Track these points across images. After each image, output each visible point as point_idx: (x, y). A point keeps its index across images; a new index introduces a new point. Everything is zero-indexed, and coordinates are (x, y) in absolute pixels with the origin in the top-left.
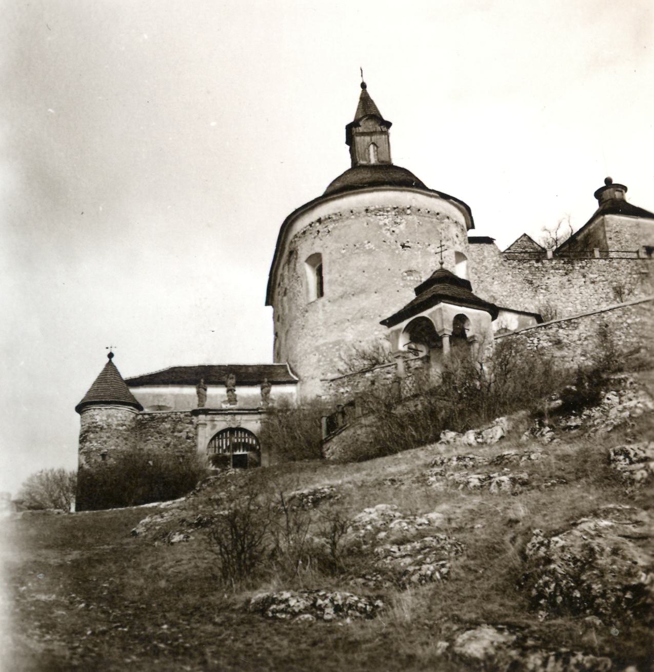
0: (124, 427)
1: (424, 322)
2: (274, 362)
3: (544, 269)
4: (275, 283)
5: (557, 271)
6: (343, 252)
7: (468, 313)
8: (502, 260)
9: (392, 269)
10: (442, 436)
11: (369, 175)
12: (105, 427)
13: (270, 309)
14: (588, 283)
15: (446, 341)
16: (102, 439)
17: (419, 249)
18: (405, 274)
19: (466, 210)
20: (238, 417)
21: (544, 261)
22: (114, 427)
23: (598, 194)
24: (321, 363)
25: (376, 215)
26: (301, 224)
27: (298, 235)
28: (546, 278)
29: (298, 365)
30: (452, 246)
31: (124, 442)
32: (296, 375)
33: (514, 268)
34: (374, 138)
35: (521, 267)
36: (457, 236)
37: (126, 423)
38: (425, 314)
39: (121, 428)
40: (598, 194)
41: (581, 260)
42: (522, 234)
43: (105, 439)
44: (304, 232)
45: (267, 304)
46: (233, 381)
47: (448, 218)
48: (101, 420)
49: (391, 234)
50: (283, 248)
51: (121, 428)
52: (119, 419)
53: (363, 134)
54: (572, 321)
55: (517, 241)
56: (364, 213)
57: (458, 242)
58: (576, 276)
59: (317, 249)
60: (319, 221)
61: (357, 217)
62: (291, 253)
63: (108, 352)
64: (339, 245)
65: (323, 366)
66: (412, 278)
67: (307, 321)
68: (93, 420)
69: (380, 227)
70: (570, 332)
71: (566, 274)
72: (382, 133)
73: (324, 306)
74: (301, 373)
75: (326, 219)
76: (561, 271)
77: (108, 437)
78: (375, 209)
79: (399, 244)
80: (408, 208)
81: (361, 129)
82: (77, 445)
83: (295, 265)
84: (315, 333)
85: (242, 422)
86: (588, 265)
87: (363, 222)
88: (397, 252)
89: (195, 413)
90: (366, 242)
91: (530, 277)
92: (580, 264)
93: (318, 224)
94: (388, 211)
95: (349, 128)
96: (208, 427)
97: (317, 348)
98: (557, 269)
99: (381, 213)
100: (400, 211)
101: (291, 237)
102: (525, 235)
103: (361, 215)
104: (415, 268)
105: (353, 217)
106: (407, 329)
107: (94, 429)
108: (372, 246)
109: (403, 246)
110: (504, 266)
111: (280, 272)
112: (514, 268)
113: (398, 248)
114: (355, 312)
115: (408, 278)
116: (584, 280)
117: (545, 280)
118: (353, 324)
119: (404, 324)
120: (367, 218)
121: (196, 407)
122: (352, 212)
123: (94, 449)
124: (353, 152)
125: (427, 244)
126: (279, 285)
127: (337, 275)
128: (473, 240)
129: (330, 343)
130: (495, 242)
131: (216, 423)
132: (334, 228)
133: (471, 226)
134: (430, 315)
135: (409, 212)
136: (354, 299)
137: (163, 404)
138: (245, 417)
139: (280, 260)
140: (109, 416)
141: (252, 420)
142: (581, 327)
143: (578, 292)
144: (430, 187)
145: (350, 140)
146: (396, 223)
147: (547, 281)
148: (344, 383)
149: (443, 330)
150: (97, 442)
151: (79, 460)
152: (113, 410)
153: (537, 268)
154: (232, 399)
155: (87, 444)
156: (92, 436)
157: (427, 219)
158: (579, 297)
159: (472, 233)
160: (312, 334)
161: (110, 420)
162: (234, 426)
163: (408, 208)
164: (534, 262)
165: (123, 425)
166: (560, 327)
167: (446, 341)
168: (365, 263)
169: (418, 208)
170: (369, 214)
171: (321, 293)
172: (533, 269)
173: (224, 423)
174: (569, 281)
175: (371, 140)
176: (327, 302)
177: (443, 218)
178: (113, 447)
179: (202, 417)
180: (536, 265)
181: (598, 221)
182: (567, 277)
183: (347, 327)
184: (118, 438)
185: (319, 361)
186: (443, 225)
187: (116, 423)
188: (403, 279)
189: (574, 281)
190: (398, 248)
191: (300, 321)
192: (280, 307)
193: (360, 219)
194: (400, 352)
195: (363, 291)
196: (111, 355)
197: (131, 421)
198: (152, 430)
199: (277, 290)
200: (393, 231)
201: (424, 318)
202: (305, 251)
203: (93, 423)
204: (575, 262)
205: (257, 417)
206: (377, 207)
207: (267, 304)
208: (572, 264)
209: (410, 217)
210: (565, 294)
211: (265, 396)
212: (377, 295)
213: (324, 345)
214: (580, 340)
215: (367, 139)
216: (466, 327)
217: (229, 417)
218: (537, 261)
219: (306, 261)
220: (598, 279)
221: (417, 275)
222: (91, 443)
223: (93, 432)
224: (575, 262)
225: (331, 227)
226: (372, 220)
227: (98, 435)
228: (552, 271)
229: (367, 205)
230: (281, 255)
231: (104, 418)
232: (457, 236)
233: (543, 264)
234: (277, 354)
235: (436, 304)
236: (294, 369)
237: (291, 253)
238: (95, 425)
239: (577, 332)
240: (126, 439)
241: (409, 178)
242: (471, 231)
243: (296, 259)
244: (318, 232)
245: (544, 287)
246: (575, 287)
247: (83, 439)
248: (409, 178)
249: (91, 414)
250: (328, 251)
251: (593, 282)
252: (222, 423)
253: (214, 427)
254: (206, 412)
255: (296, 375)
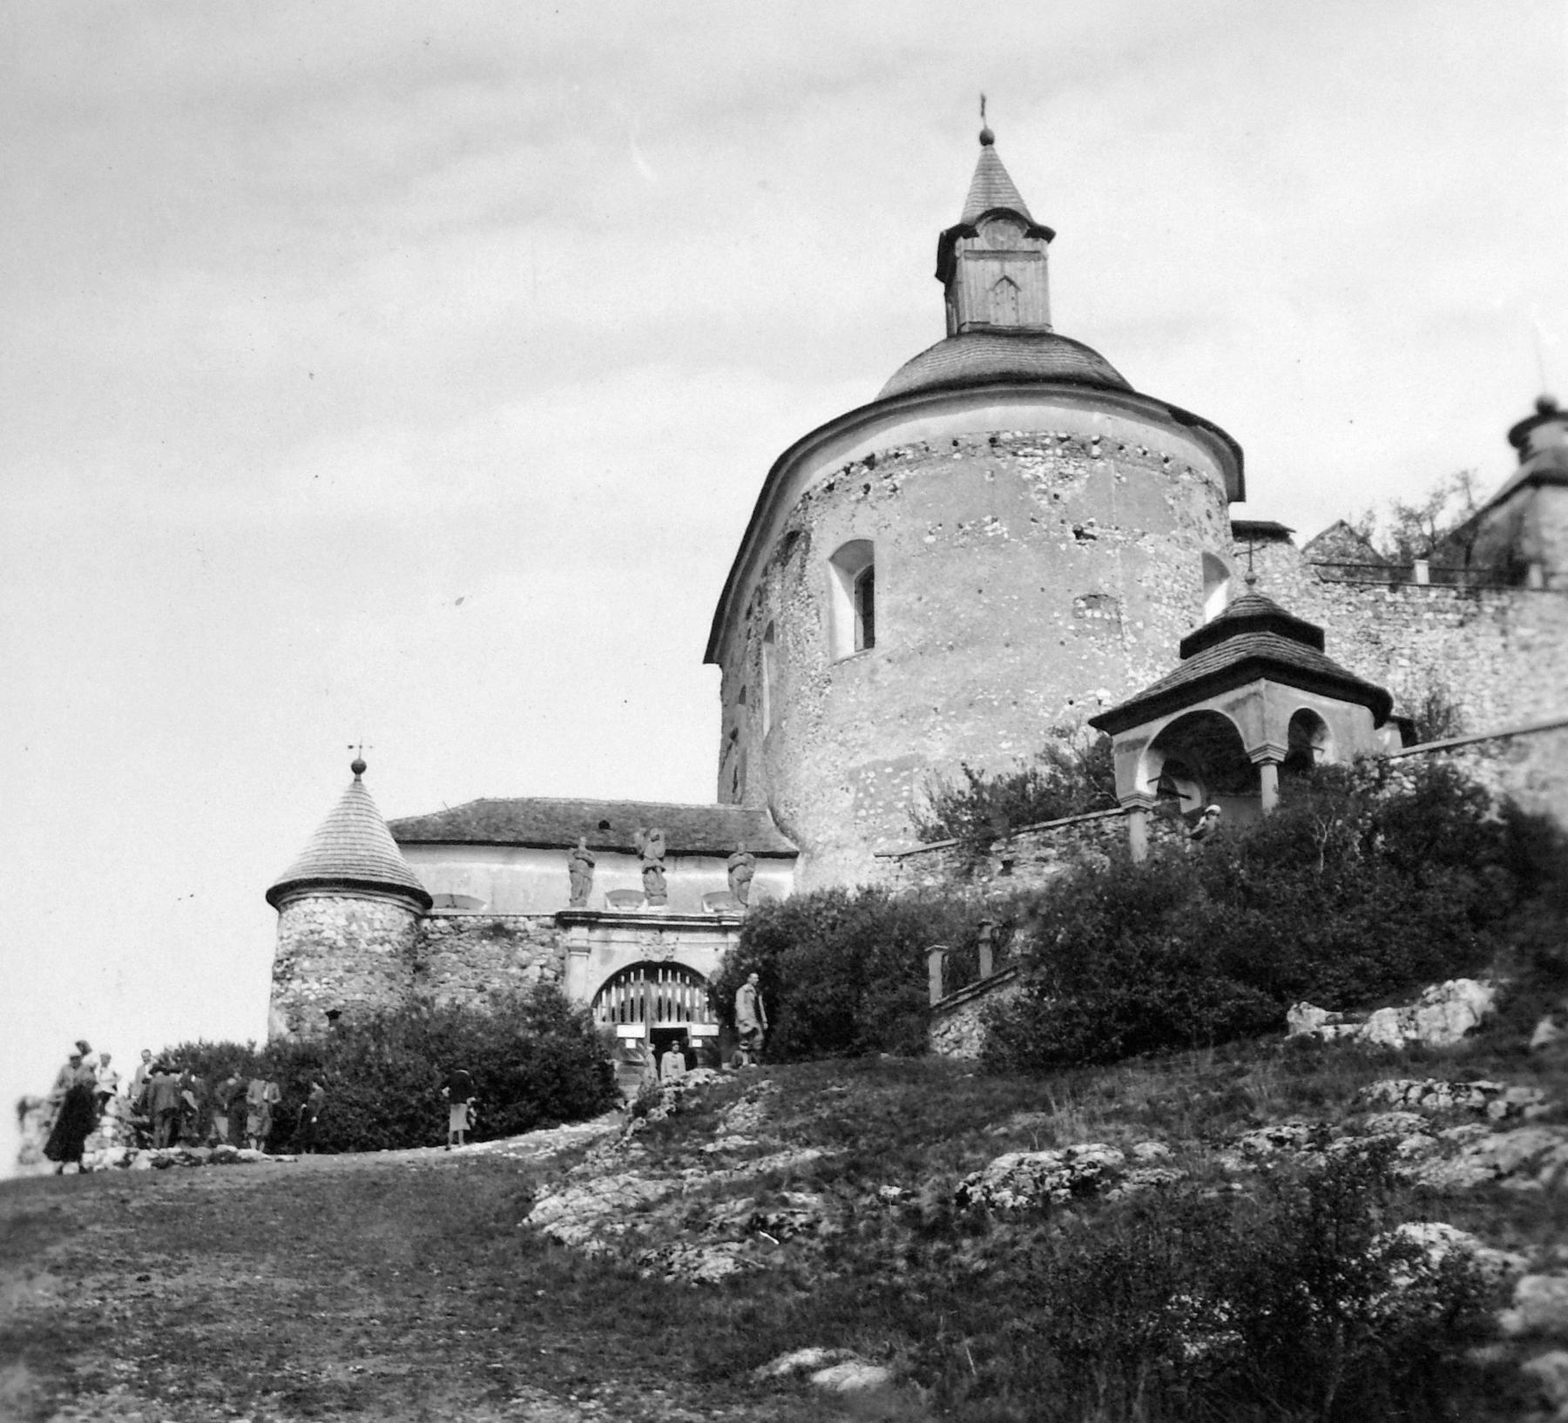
0: (388, 947)
1: (1205, 724)
2: (720, 800)
3: (1409, 609)
4: (735, 609)
5: (1441, 617)
6: (930, 539)
7: (1320, 708)
8: (1308, 581)
9: (1049, 588)
10: (1292, 1017)
11: (1000, 355)
12: (342, 943)
13: (714, 671)
14: (1513, 649)
15: (1270, 776)
16: (333, 974)
17: (1117, 542)
18: (1082, 604)
19: (1230, 455)
20: (669, 937)
21: (1409, 590)
22: (363, 945)
23: (1519, 437)
24: (863, 813)
25: (1015, 454)
26: (820, 472)
27: (814, 494)
28: (1413, 629)
29: (801, 813)
30: (1196, 539)
31: (387, 984)
32: (795, 838)
33: (1336, 601)
34: (1011, 268)
35: (1353, 600)
36: (1209, 517)
37: (394, 936)
38: (1215, 704)
39: (378, 949)
40: (1519, 437)
41: (1499, 590)
42: (1334, 521)
43: (340, 973)
44: (830, 487)
45: (708, 659)
46: (660, 848)
47: (1189, 470)
48: (336, 928)
49: (1051, 503)
50: (766, 529)
51: (378, 949)
52: (377, 925)
53: (981, 254)
54: (1515, 739)
55: (1321, 537)
56: (986, 447)
57: (1212, 532)
58: (1483, 630)
59: (863, 531)
60: (870, 462)
61: (968, 456)
62: (792, 537)
63: (353, 757)
64: (919, 523)
65: (865, 819)
66: (1097, 614)
67: (828, 704)
68: (313, 927)
69: (1025, 485)
70: (1507, 767)
71: (1462, 624)
72: (1037, 255)
73: (874, 671)
74: (800, 828)
75: (887, 458)
76: (1450, 616)
77: (349, 971)
78: (1015, 440)
79: (1069, 529)
80: (1095, 443)
81: (979, 243)
82: (267, 985)
83: (803, 567)
84: (850, 735)
85: (679, 948)
86: (1516, 606)
87: (982, 470)
88: (1063, 547)
89: (564, 921)
90: (988, 519)
91: (1374, 628)
92: (1496, 603)
93: (866, 470)
94: (1044, 447)
95: (948, 242)
96: (595, 957)
97: (853, 776)
98: (1440, 611)
99: (1029, 450)
100: (1075, 447)
101: (794, 497)
102: (1342, 524)
103: (979, 453)
104: (1106, 588)
105: (957, 456)
106: (1160, 744)
107: (310, 948)
108: (1002, 529)
109: (1079, 534)
110: (1313, 597)
111: (755, 579)
112: (1336, 601)
113: (1065, 539)
114: (951, 693)
115: (1089, 613)
116: (1502, 640)
117: (1409, 635)
118: (948, 719)
119: (1157, 727)
120: (990, 459)
121: (564, 906)
122: (955, 443)
123: (312, 997)
124: (950, 295)
125: (1138, 531)
126: (749, 613)
127: (912, 597)
128: (1243, 531)
129: (886, 764)
130: (1292, 536)
131: (613, 946)
132: (908, 481)
133: (1237, 492)
134: (1232, 707)
135: (1096, 450)
136: (952, 658)
137: (463, 892)
138: (686, 937)
139: (755, 553)
140: (351, 917)
141: (707, 945)
142: (1535, 759)
143: (1487, 668)
144: (1138, 389)
145: (947, 270)
146: (1063, 476)
147: (1415, 639)
148: (933, 865)
149: (1264, 749)
150: (319, 980)
151: (270, 1021)
152: (363, 903)
153: (1393, 604)
154: (656, 894)
155: (296, 984)
156: (306, 964)
157: (1138, 469)
158: (1491, 682)
159: (1238, 512)
160: (840, 737)
161: (354, 927)
162: (657, 958)
163: (1095, 443)
164: (1385, 590)
165: (383, 942)
166: (1484, 753)
167: (1270, 776)
168: (983, 571)
169: (1119, 440)
170: (998, 451)
171: (869, 641)
172: (1383, 608)
173: (634, 948)
174: (1467, 639)
175: (1002, 270)
176: (883, 662)
177: (1176, 472)
178: (359, 997)
179: (578, 935)
180: (1389, 598)
181: (1518, 500)
182: (1462, 632)
183: (933, 727)
184: (371, 973)
185: (858, 806)
186: (1177, 489)
187: (369, 935)
188: (1076, 614)
189: (1480, 642)
190: (1065, 539)
191: (813, 705)
192: (748, 666)
193: (974, 461)
194: (1139, 796)
195: (971, 641)
196: (358, 768)
197: (403, 934)
198: (454, 957)
199: (742, 625)
200: (1056, 496)
201: (1211, 716)
202: (828, 532)
203: (312, 932)
204: (1484, 594)
205: (715, 938)
206: (1019, 434)
207: (708, 659)
208: (1478, 600)
209: (1100, 464)
210: (1455, 672)
211: (740, 887)
212: (1010, 650)
213: (873, 766)
214: (1531, 788)
215: (993, 267)
216: (1314, 744)
217: (647, 936)
218: (1393, 588)
219: (832, 559)
220: (1539, 639)
221: (1112, 607)
222: (305, 981)
223: (310, 956)
224: (1484, 594)
225: (900, 477)
226: (1004, 466)
227: (322, 963)
228: (1429, 615)
229: (994, 430)
230: (761, 541)
231: (342, 922)
232: (1209, 517)
233: (1406, 596)
234: (732, 780)
235: (1251, 680)
236: (789, 824)
237: (792, 537)
238: (316, 937)
239: (1523, 769)
240: (390, 976)
241: (1096, 367)
242: (1234, 506)
243: (807, 551)
244: (867, 487)
245: (1407, 652)
246: (1483, 656)
247: (282, 976)
248: (1096, 367)
249: (306, 909)
250: (890, 535)
251: (1526, 647)
252: (628, 948)
253: (607, 957)
254: (591, 921)
255: (795, 838)
